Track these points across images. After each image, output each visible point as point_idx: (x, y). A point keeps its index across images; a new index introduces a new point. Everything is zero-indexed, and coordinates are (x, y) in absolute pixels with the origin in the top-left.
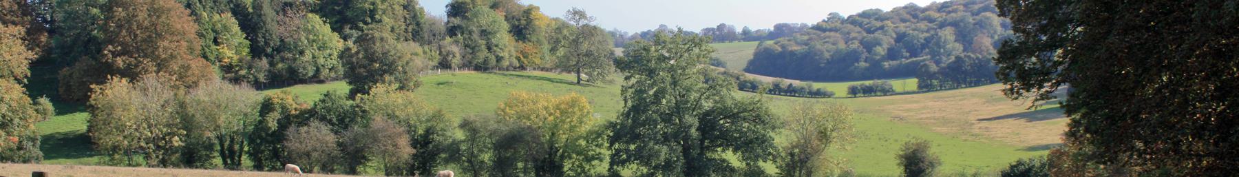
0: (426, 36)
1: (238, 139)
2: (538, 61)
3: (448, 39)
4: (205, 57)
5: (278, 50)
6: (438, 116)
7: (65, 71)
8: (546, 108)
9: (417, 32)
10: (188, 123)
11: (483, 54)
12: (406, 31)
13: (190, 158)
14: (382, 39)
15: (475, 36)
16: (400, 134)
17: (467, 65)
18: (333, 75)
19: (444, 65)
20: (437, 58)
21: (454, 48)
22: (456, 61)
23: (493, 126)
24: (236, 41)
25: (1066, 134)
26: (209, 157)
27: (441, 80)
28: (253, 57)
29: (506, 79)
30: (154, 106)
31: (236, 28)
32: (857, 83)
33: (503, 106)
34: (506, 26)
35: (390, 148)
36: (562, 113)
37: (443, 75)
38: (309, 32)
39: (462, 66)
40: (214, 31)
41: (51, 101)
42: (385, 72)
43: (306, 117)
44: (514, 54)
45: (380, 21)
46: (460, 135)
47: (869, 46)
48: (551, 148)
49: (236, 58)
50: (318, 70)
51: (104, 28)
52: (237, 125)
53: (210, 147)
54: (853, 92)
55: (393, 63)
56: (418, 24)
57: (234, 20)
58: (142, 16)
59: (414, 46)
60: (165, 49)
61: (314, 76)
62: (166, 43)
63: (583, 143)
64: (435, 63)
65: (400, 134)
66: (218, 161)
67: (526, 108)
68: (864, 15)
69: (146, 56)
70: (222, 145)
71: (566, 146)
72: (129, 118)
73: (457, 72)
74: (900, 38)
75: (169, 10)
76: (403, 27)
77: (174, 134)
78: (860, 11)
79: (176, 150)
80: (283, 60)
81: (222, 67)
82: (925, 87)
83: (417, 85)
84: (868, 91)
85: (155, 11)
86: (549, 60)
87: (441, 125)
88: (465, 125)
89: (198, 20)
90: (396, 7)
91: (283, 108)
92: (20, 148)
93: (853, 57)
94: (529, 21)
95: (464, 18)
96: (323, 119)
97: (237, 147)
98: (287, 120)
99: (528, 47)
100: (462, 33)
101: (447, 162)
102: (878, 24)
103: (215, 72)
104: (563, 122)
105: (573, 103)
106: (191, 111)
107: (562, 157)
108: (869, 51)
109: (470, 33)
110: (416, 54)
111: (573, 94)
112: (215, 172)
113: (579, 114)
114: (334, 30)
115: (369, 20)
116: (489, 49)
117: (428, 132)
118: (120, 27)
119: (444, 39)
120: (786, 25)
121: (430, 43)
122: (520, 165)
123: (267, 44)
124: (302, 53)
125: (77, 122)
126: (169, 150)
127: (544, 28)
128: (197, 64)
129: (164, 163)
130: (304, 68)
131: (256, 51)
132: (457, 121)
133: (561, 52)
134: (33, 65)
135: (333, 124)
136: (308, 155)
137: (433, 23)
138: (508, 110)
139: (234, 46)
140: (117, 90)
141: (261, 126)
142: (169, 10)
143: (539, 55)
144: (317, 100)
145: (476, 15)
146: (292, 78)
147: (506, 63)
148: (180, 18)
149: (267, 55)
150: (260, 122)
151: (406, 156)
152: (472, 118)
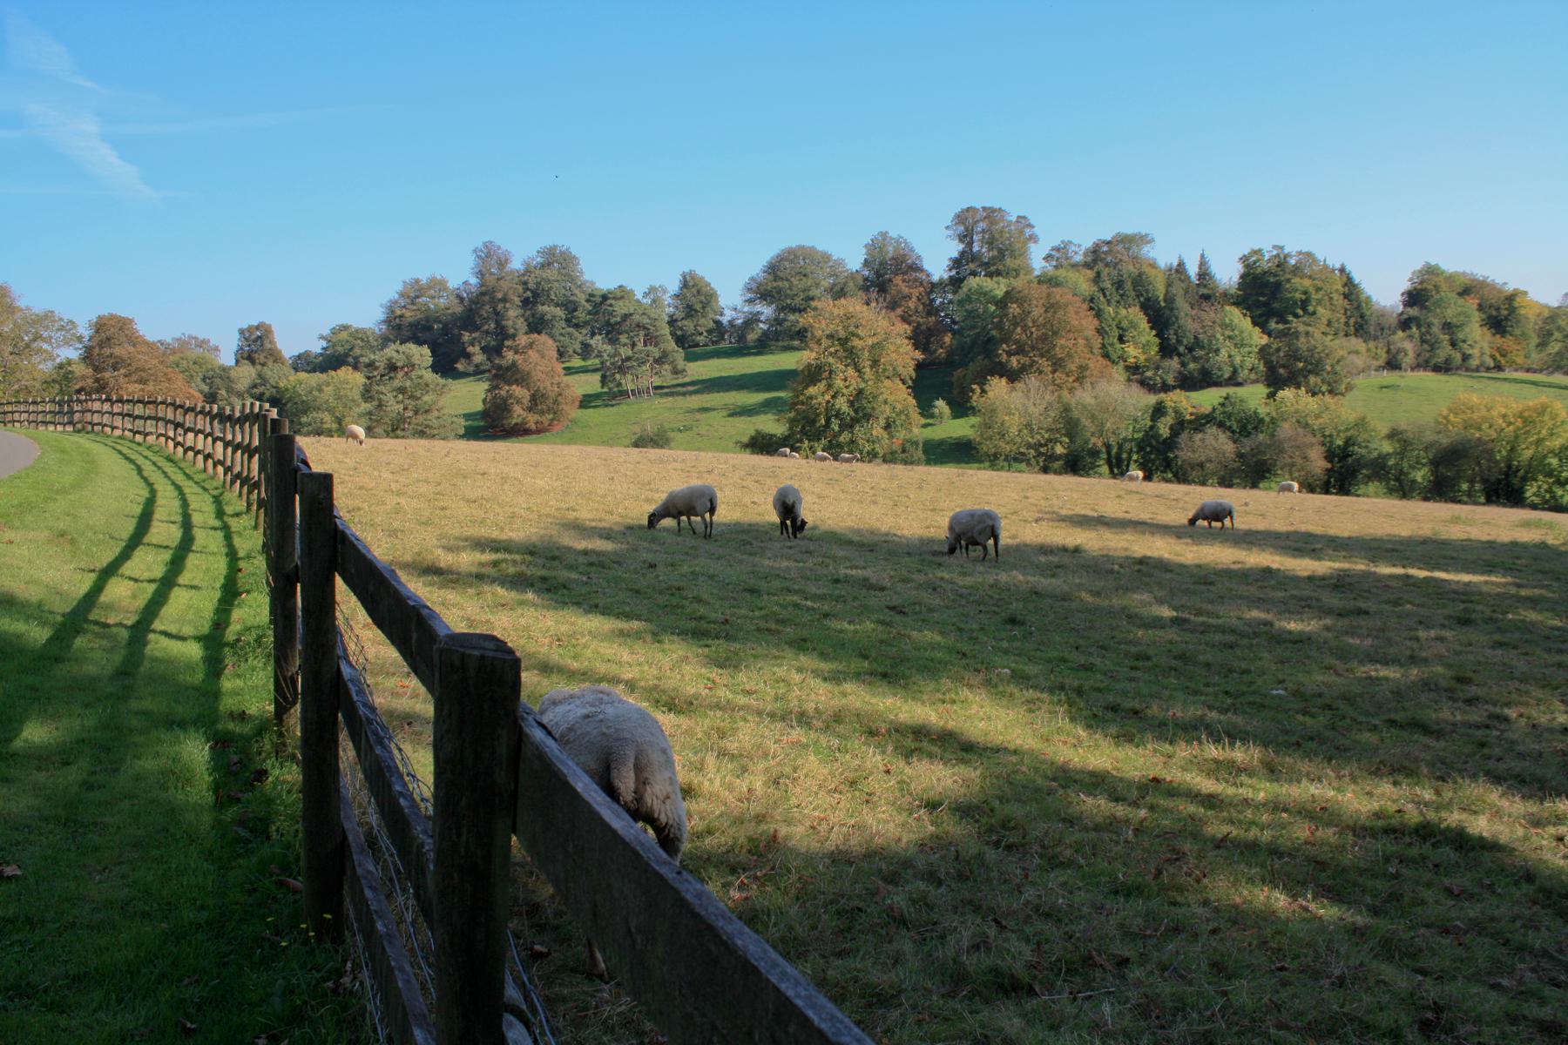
0: (1372, 329)
1: (1127, 446)
2: (1520, 360)
3: (1400, 334)
4: (1106, 356)
5: (1190, 349)
6: (1361, 423)
7: (959, 372)
8: (1504, 416)
9: (1361, 326)
10: (1071, 427)
11: (1444, 351)
12: (1347, 324)
13: (1075, 464)
14: (1307, 333)
15: (1436, 330)
16: (1312, 445)
17: (1422, 364)
18: (1253, 376)
19: (1393, 365)
20: (1384, 356)
21: (1407, 345)
22: (1409, 359)
23: (1429, 437)
24: (1143, 340)
25: (417, 281)
26: (1093, 466)
27: (1385, 383)
28: (1163, 357)
29: (1470, 382)
30: (1035, 411)
31: (1144, 324)
33: (1445, 412)
34: (1477, 317)
35: (1299, 461)
36: (1525, 421)
37: (1389, 377)
38: (1224, 326)
39: (1417, 367)
40: (1118, 327)
41: (949, 404)
42: (1310, 372)
43: (1201, 422)
44: (1487, 351)
45: (1314, 313)
46: (1387, 447)
48: (1509, 467)
49: (1142, 358)
50: (1235, 371)
51: (999, 326)
52: (1127, 432)
53: (1094, 453)
55: (1320, 361)
56: (1362, 317)
57: (1141, 315)
58: (1037, 312)
59: (1357, 343)
60: (1062, 347)
61: (1230, 378)
62: (1063, 342)
63: (1554, 462)
64: (1381, 362)
65: (1312, 445)
66: (1105, 469)
67: (1475, 416)
69: (1042, 356)
70: (1109, 453)
71: (1530, 465)
72: (1013, 424)
73: (1409, 373)
75: (1066, 305)
76: (1343, 320)
77: (1056, 441)
79: (1058, 458)
80: (1195, 359)
81: (1127, 368)
83: (1350, 388)
85: (1052, 306)
86: (1536, 358)
87: (1364, 436)
88: (1393, 435)
89: (1099, 315)
90: (1335, 296)
91: (1176, 412)
92: (904, 451)
94: (1512, 310)
95: (1423, 307)
96: (1221, 425)
97: (1124, 456)
98: (1180, 426)
99: (1508, 342)
100: (1419, 327)
101: (1369, 479)
103: (1118, 373)
104: (1527, 432)
105: (1541, 411)
106: (1075, 414)
107: (1524, 479)
109: (1429, 325)
110: (1357, 353)
111: (1544, 399)
112: (1132, 486)
113: (1550, 423)
114: (1255, 323)
115: (1300, 312)
116: (1453, 344)
117: (1349, 442)
118: (1016, 325)
119: (1394, 333)
121: (1376, 338)
122: (1465, 486)
123: (1179, 342)
124: (1217, 351)
125: (961, 428)
126: (1052, 457)
127: (1532, 318)
128: (1096, 363)
129: (1045, 470)
130: (1220, 369)
131: (1166, 350)
132: (1384, 430)
133: (1555, 347)
134: (919, 367)
135: (1233, 432)
136: (1201, 465)
137: (1382, 314)
138: (1452, 417)
139: (1141, 344)
140: (998, 387)
141: (1151, 433)
142: (1066, 305)
143: (1522, 353)
144: (1216, 403)
145: (1438, 304)
146: (1205, 380)
147: (1474, 363)
148: (1077, 313)
149: (1179, 355)
150: (1152, 428)
151: (1318, 471)
152: (1403, 426)
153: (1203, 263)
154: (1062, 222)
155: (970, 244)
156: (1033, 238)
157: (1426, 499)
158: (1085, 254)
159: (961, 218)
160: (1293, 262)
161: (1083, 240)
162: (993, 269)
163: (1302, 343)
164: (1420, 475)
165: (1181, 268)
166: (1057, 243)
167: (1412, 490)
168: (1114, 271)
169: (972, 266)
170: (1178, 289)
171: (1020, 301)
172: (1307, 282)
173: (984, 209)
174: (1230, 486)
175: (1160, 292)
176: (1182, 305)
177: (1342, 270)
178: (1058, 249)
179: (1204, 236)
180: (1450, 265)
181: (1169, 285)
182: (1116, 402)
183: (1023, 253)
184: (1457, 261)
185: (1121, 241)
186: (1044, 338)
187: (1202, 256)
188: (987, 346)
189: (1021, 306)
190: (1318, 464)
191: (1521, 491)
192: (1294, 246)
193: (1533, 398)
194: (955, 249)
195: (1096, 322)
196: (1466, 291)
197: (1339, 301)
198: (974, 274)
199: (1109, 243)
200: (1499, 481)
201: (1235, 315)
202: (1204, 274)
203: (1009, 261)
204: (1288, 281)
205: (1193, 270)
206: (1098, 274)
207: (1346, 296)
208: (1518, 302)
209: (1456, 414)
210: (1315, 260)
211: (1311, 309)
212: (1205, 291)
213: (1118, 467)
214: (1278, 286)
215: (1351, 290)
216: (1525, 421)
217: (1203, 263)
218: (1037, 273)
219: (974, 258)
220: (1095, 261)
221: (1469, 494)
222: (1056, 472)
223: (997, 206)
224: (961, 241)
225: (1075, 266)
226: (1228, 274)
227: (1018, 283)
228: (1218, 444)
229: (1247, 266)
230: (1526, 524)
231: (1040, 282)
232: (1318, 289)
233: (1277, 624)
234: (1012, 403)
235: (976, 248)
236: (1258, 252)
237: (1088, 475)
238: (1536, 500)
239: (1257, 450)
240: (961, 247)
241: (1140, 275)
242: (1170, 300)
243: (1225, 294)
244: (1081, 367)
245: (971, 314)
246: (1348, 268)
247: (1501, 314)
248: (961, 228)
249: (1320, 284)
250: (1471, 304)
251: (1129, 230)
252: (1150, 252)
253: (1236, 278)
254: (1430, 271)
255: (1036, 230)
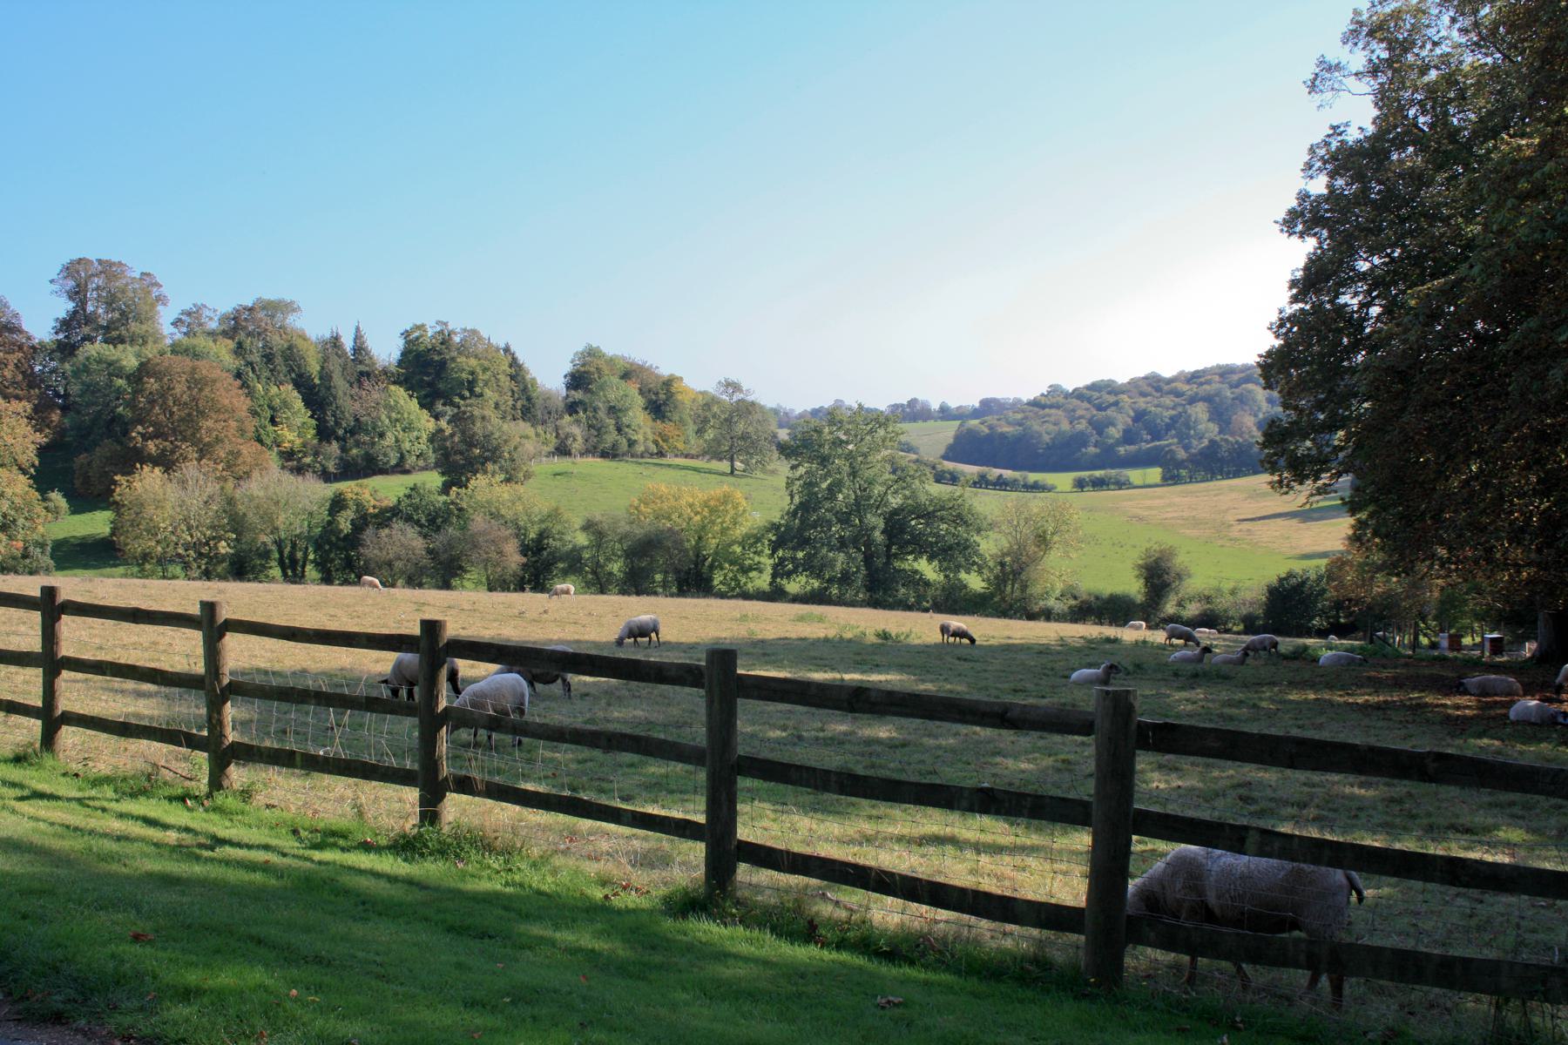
0: (539, 413)
1: (302, 544)
2: (680, 446)
3: (567, 418)
4: (260, 441)
6: (554, 515)
7: (82, 458)
8: (691, 506)
10: (237, 524)
11: (611, 437)
12: (514, 407)
14: (483, 418)
15: (602, 414)
16: (506, 539)
18: (421, 463)
19: (563, 451)
20: (554, 442)
21: (575, 430)
22: (577, 446)
23: (624, 527)
24: (298, 421)
26: (264, 568)
27: (558, 470)
29: (639, 469)
31: (298, 404)
32: (1085, 474)
33: (636, 503)
34: (640, 401)
35: (494, 555)
36: (712, 511)
38: (391, 408)
41: (65, 496)
43: (387, 516)
44: (651, 437)
45: (481, 395)
46: (582, 539)
47: (1099, 427)
49: (298, 442)
50: (402, 457)
51: (132, 405)
52: (300, 527)
53: (266, 555)
54: (1080, 485)
56: (529, 399)
57: (296, 394)
58: (179, 389)
59: (524, 427)
60: (209, 430)
61: (397, 465)
62: (210, 423)
63: (738, 549)
64: (551, 448)
65: (506, 539)
66: (276, 572)
68: (1094, 387)
69: (184, 439)
70: (281, 553)
72: (163, 518)
73: (578, 459)
74: (1139, 416)
76: (510, 403)
77: (220, 539)
78: (1088, 382)
80: (358, 444)
81: (281, 454)
82: (1170, 479)
83: (528, 476)
84: (1099, 484)
85: (197, 382)
86: (695, 444)
87: (559, 527)
88: (588, 527)
89: (251, 393)
90: (502, 377)
91: (359, 505)
93: (1079, 440)
94: (670, 395)
95: (587, 391)
96: (408, 519)
97: (299, 555)
98: (363, 521)
99: (668, 428)
100: (585, 411)
101: (565, 573)
102: (1112, 399)
103: (272, 459)
105: (726, 499)
106: (241, 509)
107: (712, 567)
108: (1100, 433)
109: (595, 410)
110: (527, 437)
111: (725, 488)
113: (732, 512)
114: (422, 406)
116: (619, 430)
117: (542, 535)
118: (152, 402)
119: (561, 417)
120: (994, 400)
121: (544, 423)
122: (658, 577)
123: (337, 423)
124: (382, 435)
125: (97, 523)
126: (215, 559)
128: (248, 450)
129: (207, 575)
130: (385, 455)
132: (578, 522)
133: (710, 434)
134: (42, 451)
135: (421, 526)
136: (390, 564)
137: (548, 397)
139: (297, 427)
140: (148, 482)
141: (330, 527)
142: (214, 381)
144: (401, 494)
146: (370, 467)
147: (640, 448)
148: (228, 391)
149: (338, 439)
150: (329, 523)
151: (514, 566)
152: (598, 518)
153: (358, 336)
154: (195, 280)
155: (82, 304)
156: (161, 299)
157: (623, 592)
158: (221, 321)
159: (71, 269)
160: (457, 339)
161: (221, 302)
162: (114, 334)
163: (478, 428)
164: (616, 567)
165: (335, 341)
166: (188, 306)
167: (609, 582)
168: (257, 340)
169: (86, 330)
170: (335, 366)
171: (159, 376)
172: (473, 362)
173: (100, 261)
174: (420, 585)
175: (314, 368)
176: (339, 383)
177: (507, 350)
178: (189, 314)
179: (361, 306)
180: (610, 349)
181: (325, 360)
182: (295, 499)
183: (146, 317)
184: (619, 345)
185: (264, 308)
186: (188, 420)
187: (358, 329)
188: (116, 428)
189: (159, 378)
190: (514, 560)
191: (710, 579)
192: (458, 323)
193: (715, 488)
194: (63, 307)
195: (248, 401)
196: (626, 376)
197: (505, 381)
198: (91, 339)
199: (251, 310)
200: (688, 572)
201: (399, 393)
202: (359, 349)
203: (134, 327)
204: (453, 359)
205: (348, 343)
206: (240, 345)
207: (512, 378)
208: (675, 387)
209: (646, 504)
210: (480, 338)
211: (477, 390)
212: (361, 368)
213: (293, 571)
214: (443, 365)
215: (517, 372)
216: (712, 511)
217: (358, 336)
218: (169, 341)
219: (89, 319)
220: (235, 329)
221: (665, 584)
222: (222, 578)
223: (115, 259)
224: (71, 298)
225: (212, 334)
226: (386, 350)
227: (150, 351)
228: (406, 540)
229: (408, 342)
230: (801, 619)
231: (173, 352)
232: (485, 370)
233: (860, 733)
234: (161, 495)
235: (90, 308)
236: (421, 327)
237: (256, 579)
238: (723, 588)
239: (450, 546)
240: (71, 305)
241: (290, 348)
242: (326, 376)
243: (385, 372)
244: (231, 453)
245: (90, 389)
246: (513, 349)
247: (661, 399)
248: (71, 283)
249: (486, 363)
250: (632, 389)
251: (270, 295)
252: (295, 322)
253: (396, 355)
254: (592, 353)
255: (164, 290)
